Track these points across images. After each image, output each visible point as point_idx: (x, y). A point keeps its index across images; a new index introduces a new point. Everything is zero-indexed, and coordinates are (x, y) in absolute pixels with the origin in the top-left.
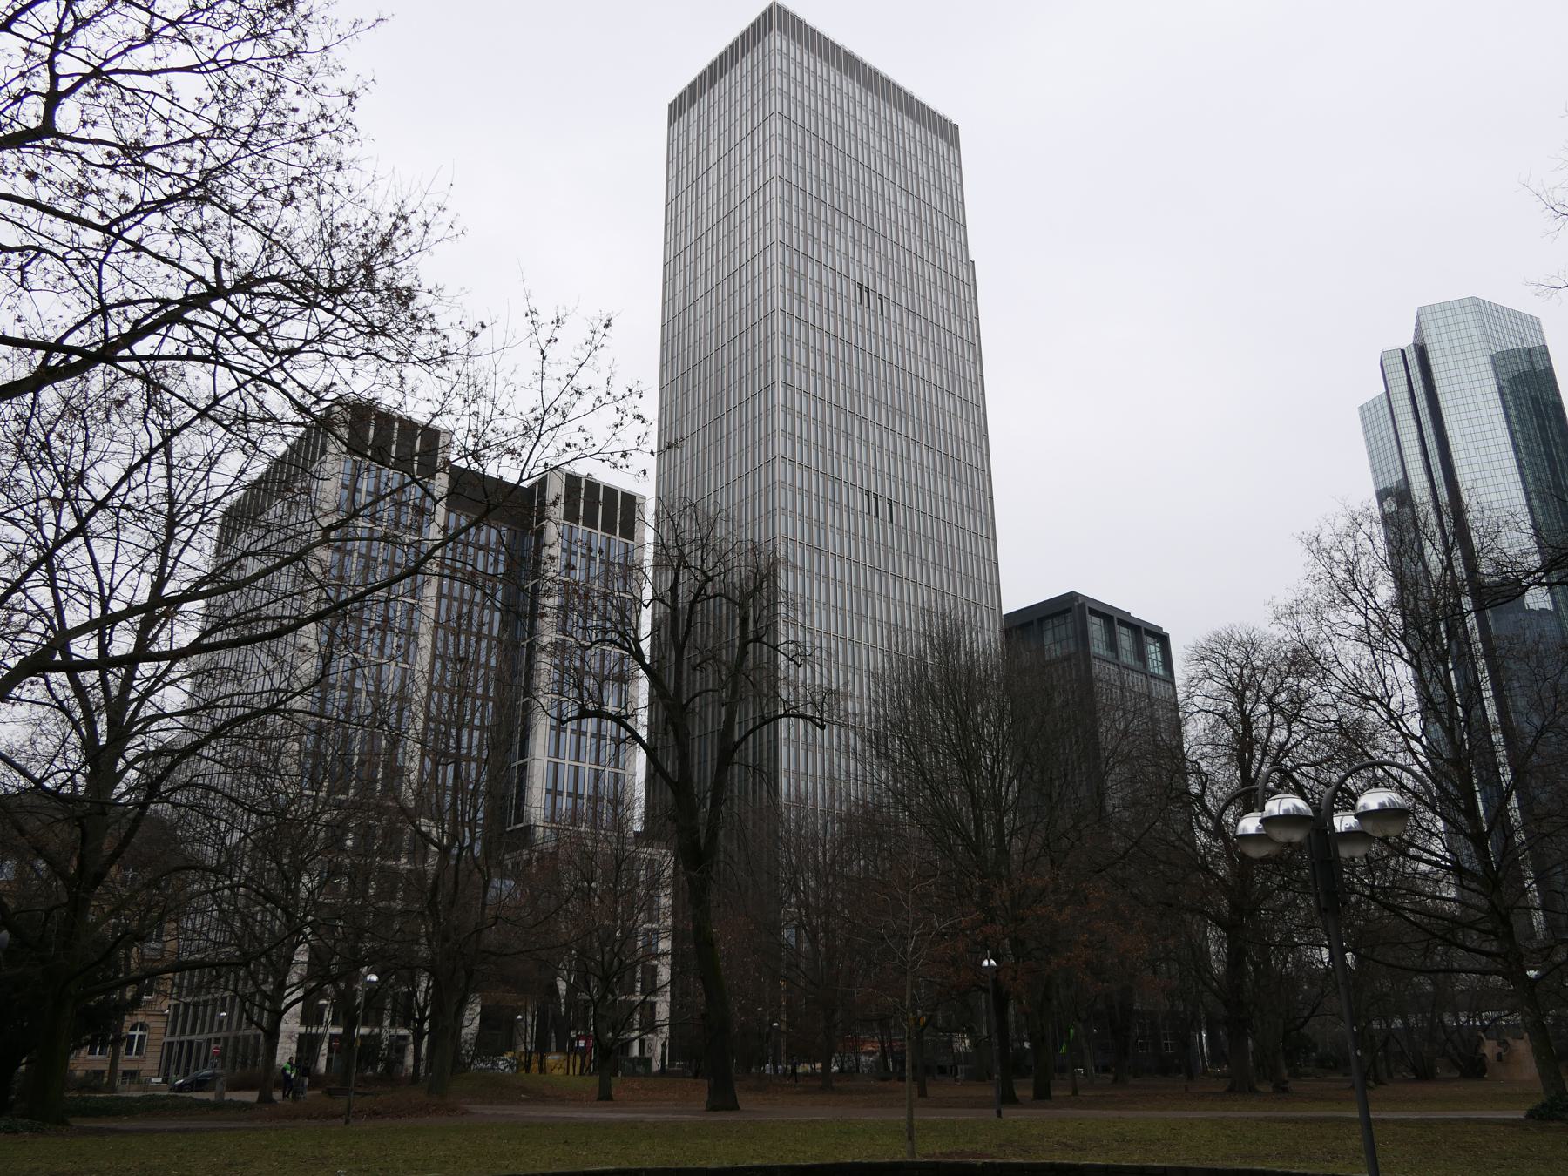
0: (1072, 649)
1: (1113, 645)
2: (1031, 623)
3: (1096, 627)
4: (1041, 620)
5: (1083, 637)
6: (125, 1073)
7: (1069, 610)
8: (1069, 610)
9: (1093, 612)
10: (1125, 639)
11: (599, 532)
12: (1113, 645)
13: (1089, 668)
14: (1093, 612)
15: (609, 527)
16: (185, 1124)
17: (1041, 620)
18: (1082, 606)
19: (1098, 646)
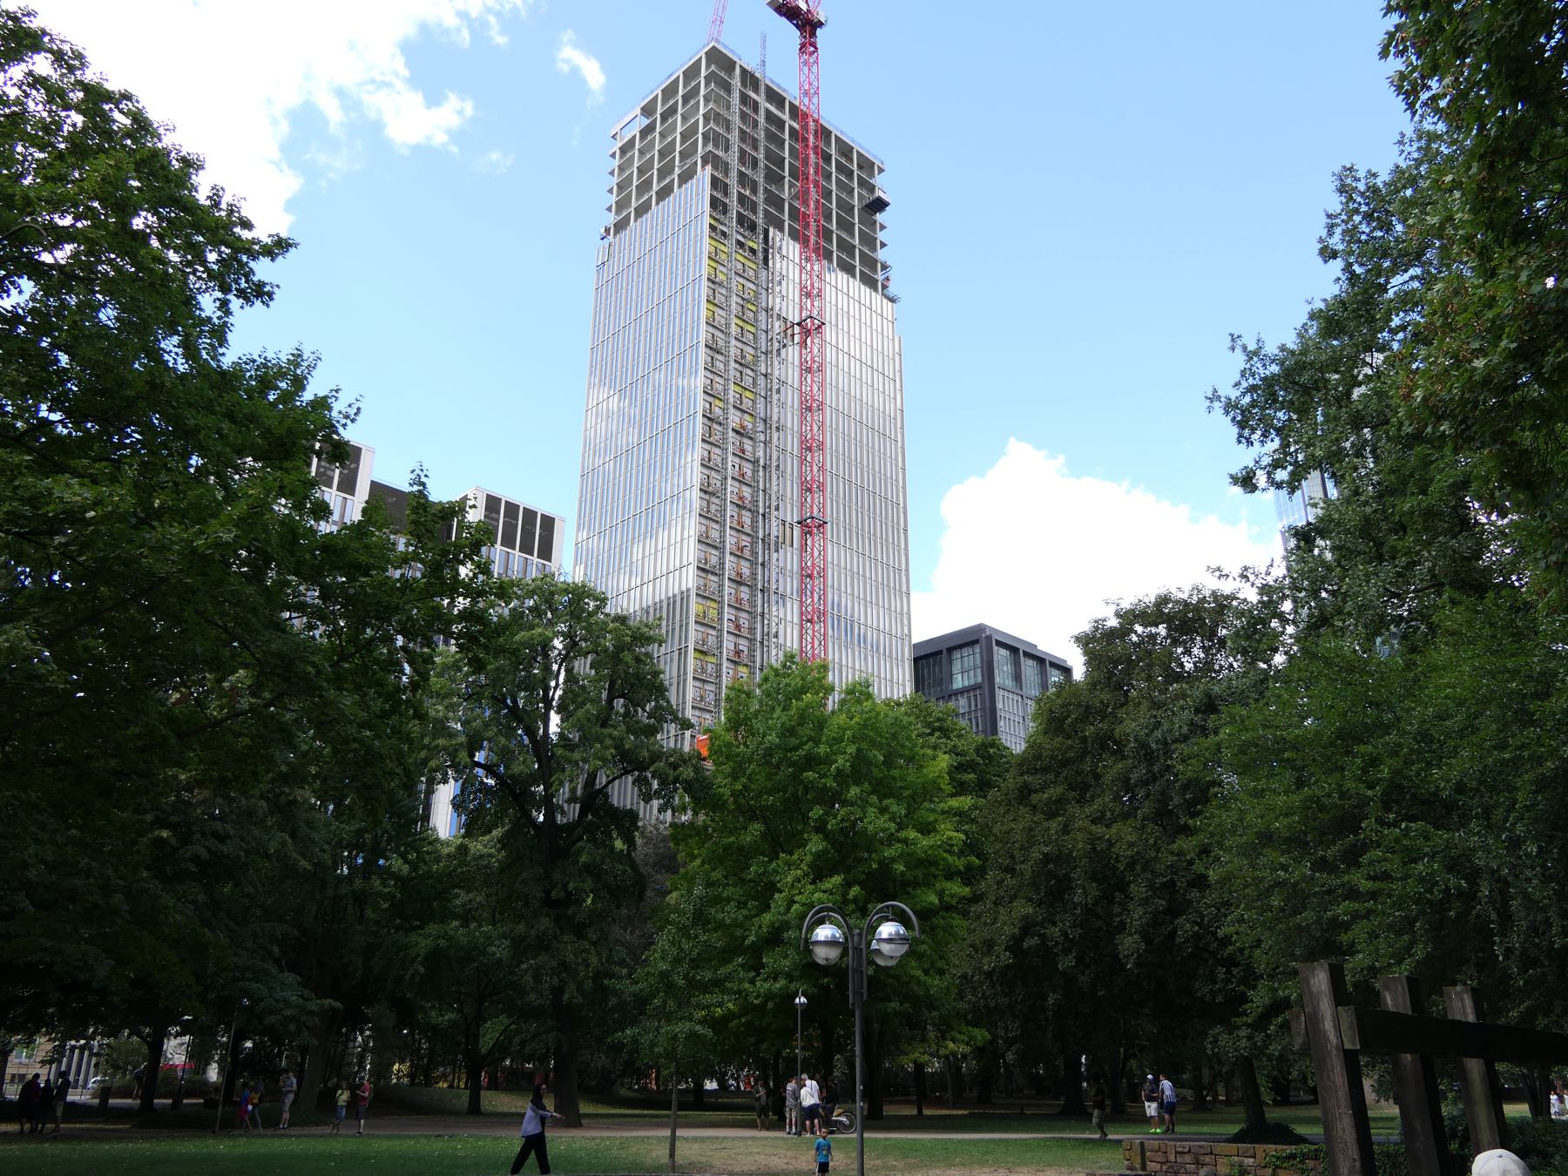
0: (979, 679)
1: (1017, 677)
2: (940, 652)
3: (1001, 654)
4: (950, 650)
5: (989, 668)
6: (13, 1076)
7: (977, 642)
8: (977, 642)
9: (1000, 644)
10: (1029, 667)
11: (517, 552)
12: (1017, 677)
13: (810, 952)
14: (1000, 644)
15: (527, 548)
16: (622, 1111)
17: (950, 650)
18: (989, 638)
19: (1003, 675)
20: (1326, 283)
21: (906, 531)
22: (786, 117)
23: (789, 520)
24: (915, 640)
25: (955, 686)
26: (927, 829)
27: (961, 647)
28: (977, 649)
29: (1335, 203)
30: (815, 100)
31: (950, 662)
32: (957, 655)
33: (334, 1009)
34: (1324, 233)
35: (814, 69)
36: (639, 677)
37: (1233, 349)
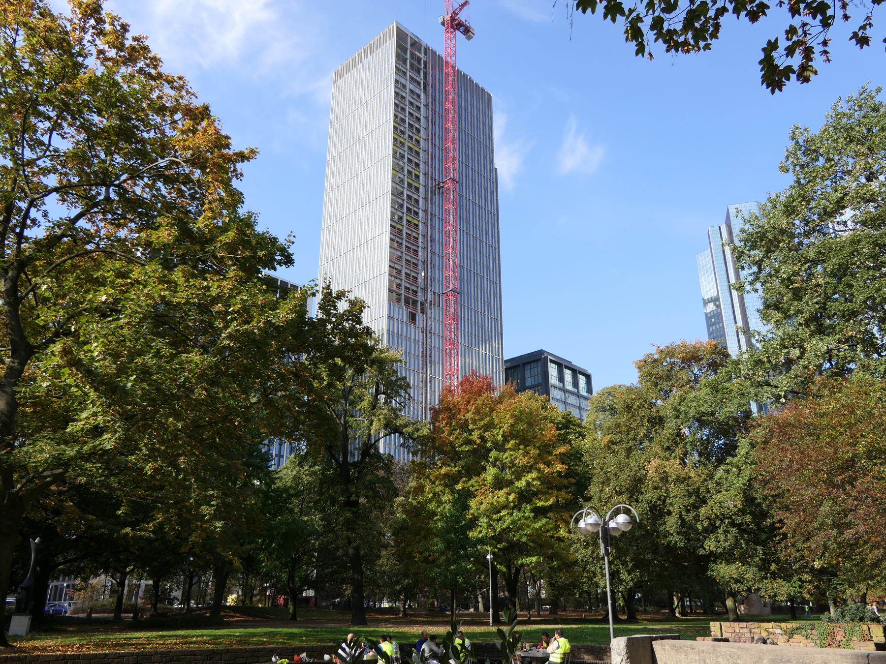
0: (540, 381)
1: (561, 379)
3: (553, 370)
4: (524, 364)
7: (539, 360)
12: (561, 379)
17: (524, 364)
20: (783, 185)
21: (500, 298)
22: (422, 56)
23: (437, 291)
24: (506, 357)
25: (527, 385)
26: (549, 464)
27: (530, 363)
28: (539, 364)
29: (791, 145)
30: (453, 58)
31: (524, 371)
32: (528, 367)
33: (14, 488)
34: (784, 160)
35: (453, 41)
36: (746, 501)
37: (641, 49)
